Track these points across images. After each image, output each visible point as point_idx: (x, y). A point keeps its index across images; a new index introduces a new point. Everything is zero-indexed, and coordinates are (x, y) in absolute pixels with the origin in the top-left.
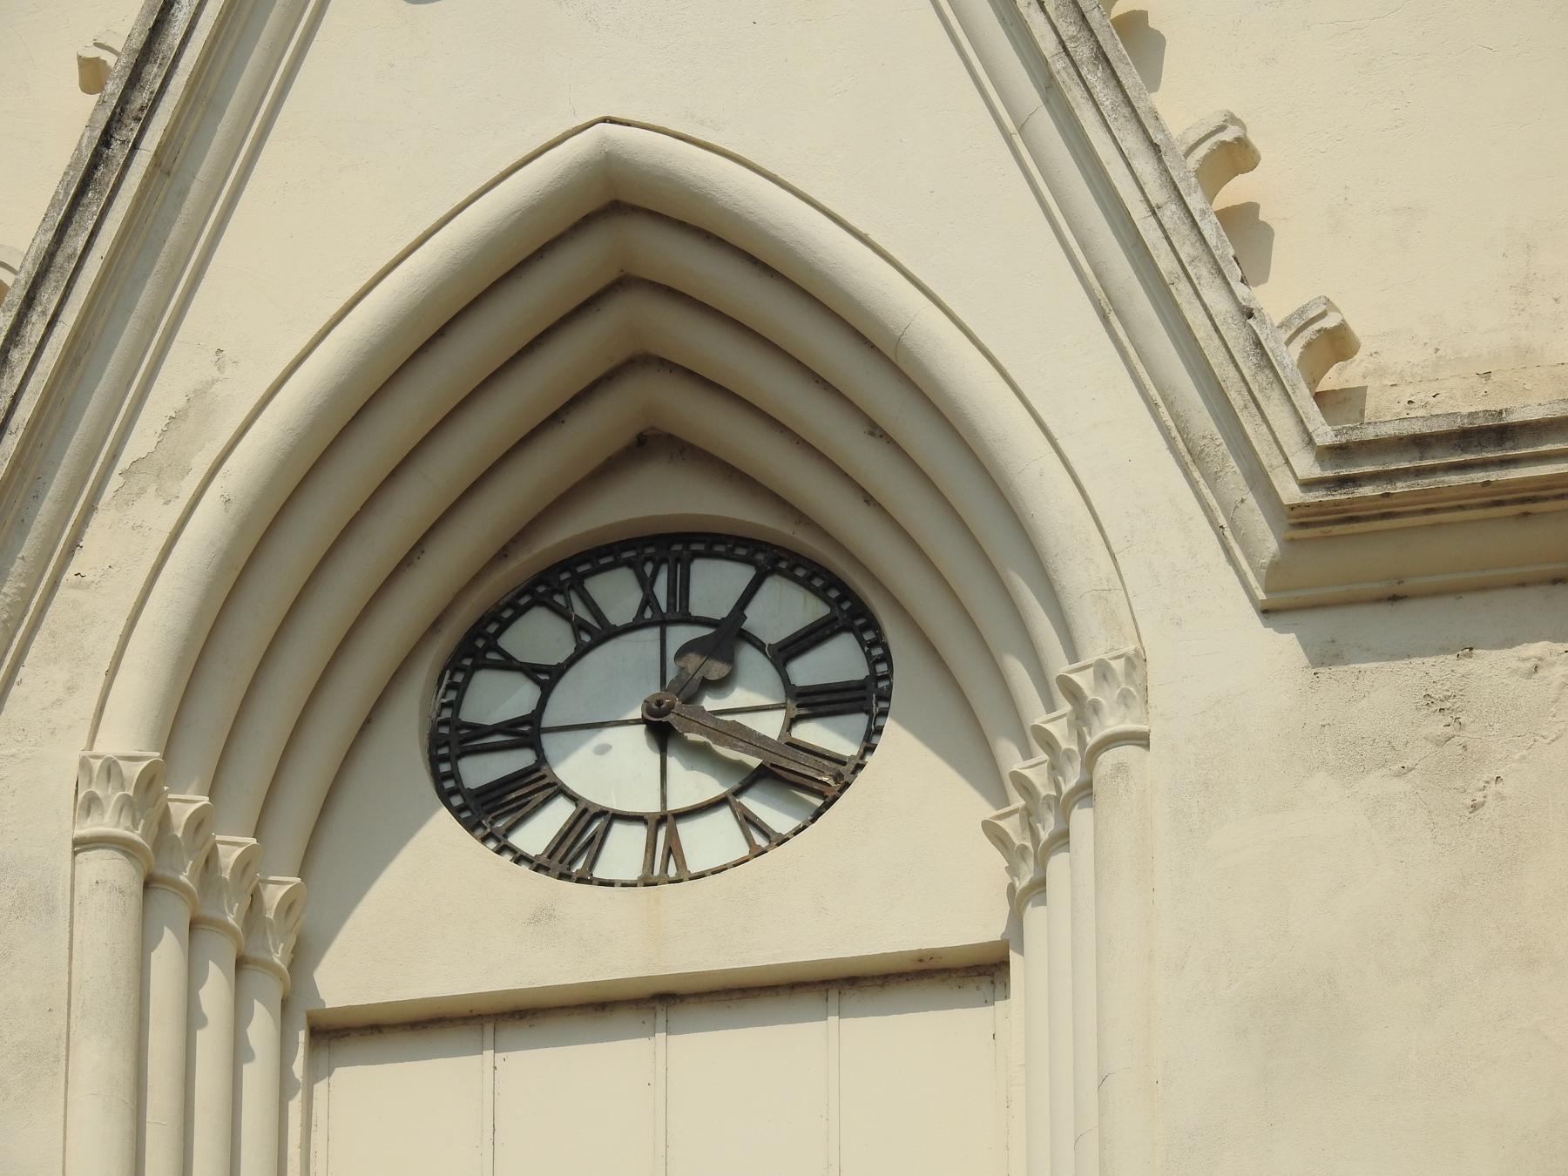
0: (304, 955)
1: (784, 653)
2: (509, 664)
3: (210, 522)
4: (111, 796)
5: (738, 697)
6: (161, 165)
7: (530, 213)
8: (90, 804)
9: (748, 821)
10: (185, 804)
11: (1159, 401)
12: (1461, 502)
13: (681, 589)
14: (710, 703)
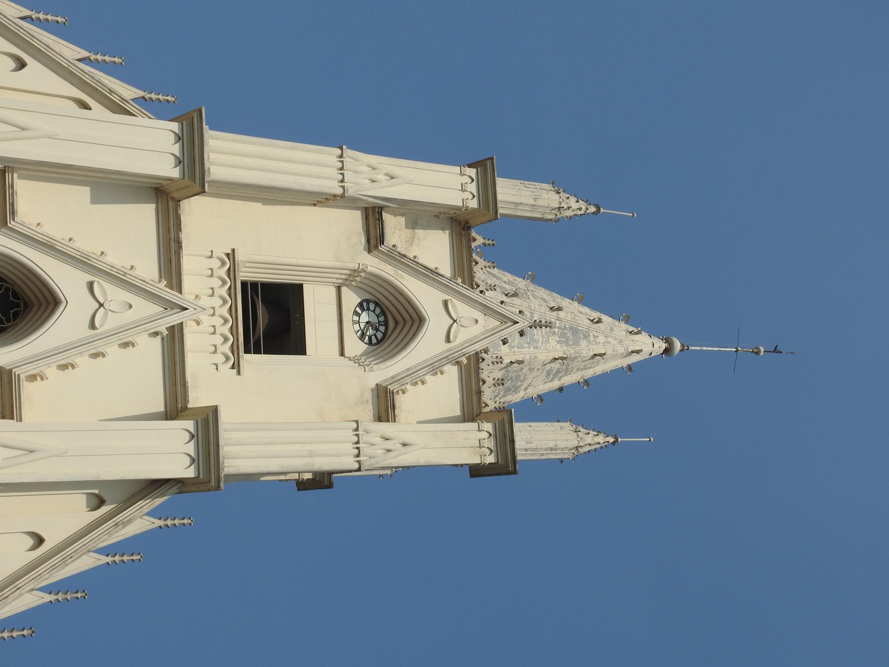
0: (347, 286)
1: (375, 335)
2: (375, 307)
3: (391, 278)
4: (364, 267)
5: (371, 330)
8: (363, 265)
9: (358, 331)
10: (363, 274)
11: (399, 374)
13: (382, 325)
14: (370, 327)
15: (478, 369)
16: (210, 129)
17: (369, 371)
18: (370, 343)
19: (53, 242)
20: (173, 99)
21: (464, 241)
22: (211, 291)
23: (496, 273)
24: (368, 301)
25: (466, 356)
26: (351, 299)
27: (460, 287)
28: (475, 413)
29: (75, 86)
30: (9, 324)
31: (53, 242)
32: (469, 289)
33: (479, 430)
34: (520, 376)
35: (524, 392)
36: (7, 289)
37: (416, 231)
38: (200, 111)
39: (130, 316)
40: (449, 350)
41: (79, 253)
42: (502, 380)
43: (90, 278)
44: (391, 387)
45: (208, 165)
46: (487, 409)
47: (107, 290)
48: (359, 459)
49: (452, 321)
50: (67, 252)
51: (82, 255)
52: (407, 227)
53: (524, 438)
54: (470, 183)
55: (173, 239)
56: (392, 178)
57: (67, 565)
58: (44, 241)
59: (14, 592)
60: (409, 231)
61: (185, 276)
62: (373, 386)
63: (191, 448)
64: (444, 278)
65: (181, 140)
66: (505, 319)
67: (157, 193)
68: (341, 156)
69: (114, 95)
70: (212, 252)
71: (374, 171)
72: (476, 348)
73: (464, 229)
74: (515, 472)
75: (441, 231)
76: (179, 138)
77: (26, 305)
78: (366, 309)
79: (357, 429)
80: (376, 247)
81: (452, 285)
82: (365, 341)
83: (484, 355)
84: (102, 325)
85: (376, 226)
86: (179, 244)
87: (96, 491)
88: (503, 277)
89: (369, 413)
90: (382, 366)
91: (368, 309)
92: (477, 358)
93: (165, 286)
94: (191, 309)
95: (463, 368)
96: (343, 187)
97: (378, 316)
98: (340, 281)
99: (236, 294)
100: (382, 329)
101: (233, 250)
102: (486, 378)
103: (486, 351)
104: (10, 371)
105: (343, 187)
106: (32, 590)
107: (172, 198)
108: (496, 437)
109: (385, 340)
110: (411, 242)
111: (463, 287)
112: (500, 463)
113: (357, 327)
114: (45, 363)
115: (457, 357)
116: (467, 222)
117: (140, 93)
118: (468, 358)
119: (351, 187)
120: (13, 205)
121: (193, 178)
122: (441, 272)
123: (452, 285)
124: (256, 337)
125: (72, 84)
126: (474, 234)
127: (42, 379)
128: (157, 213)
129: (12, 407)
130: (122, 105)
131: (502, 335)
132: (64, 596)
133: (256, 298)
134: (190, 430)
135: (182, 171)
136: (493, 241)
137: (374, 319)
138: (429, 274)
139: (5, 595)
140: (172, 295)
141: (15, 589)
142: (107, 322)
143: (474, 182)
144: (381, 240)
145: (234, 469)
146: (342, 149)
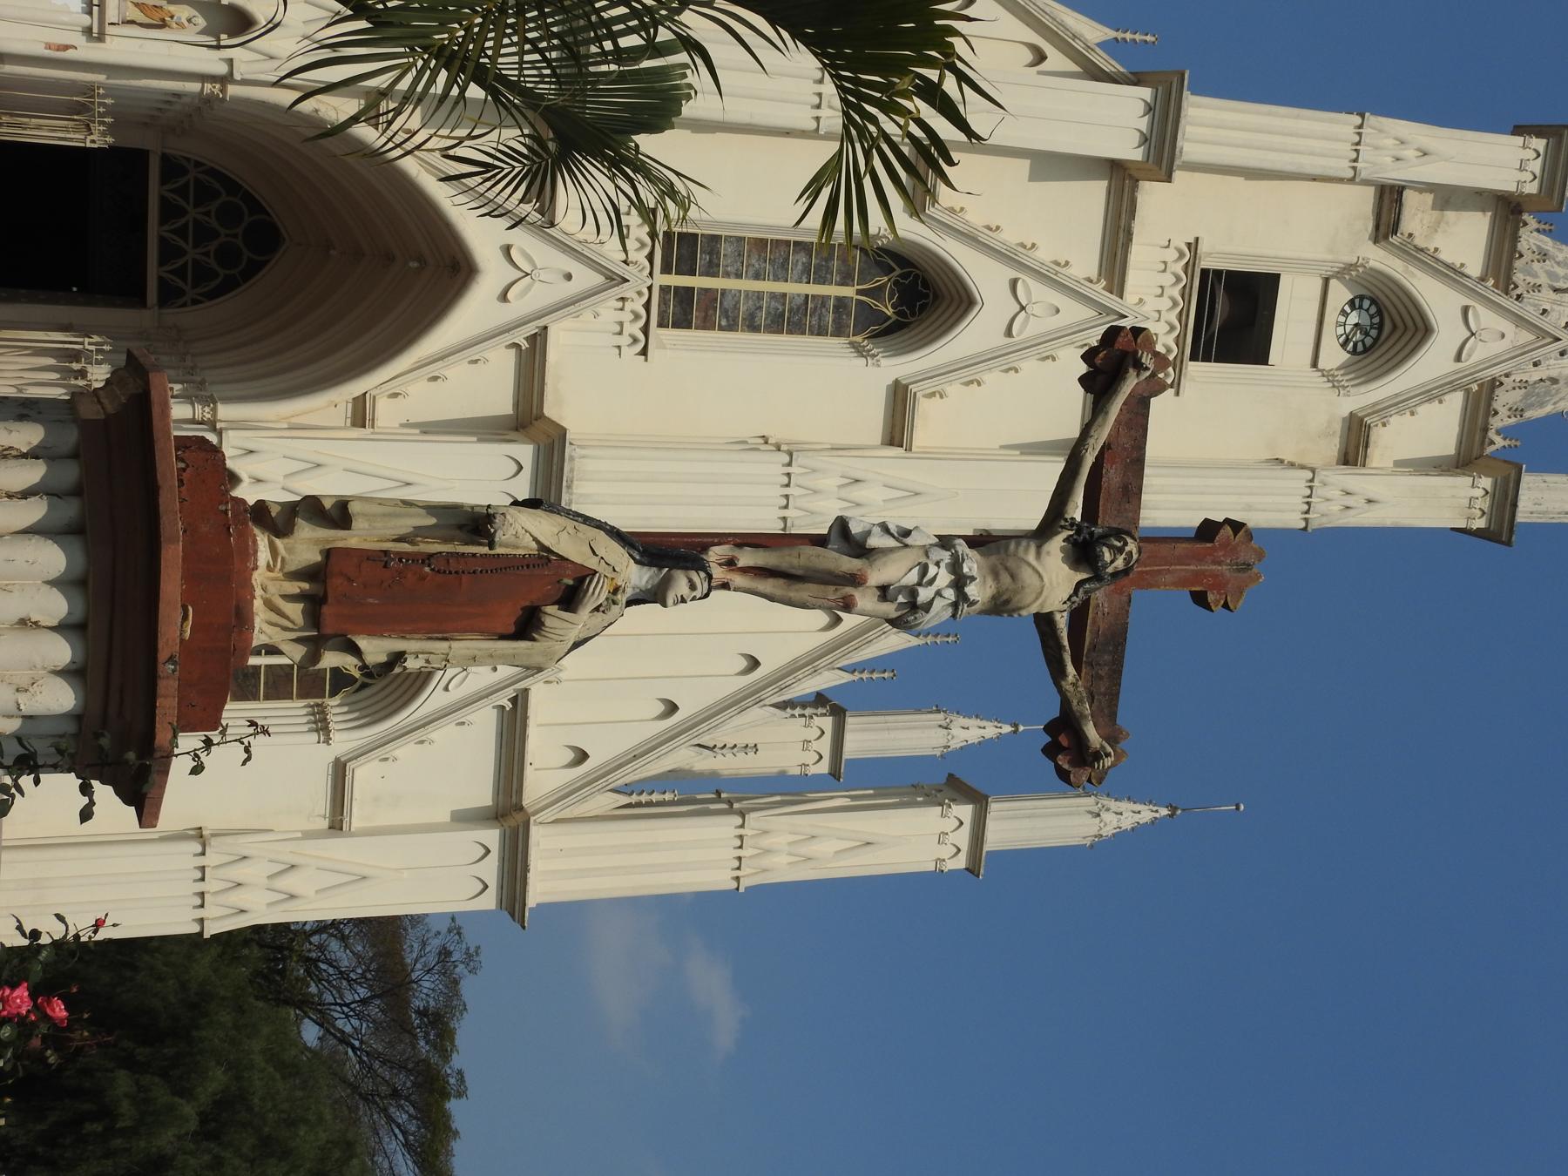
0: (1338, 278)
1: (1363, 341)
2: (1370, 306)
3: (1397, 276)
4: (1364, 262)
5: (1358, 335)
6: (1447, 275)
7: (1428, 320)
8: (1363, 259)
9: (1342, 335)
10: (1361, 270)
11: (1382, 401)
12: (1359, 440)
13: (1375, 328)
14: (1358, 332)
15: (1490, 399)
16: (1192, 94)
17: (1344, 395)
18: (1354, 352)
19: (976, 232)
20: (1153, 39)
21: (1509, 231)
22: (1160, 290)
23: (1551, 249)
24: (1362, 298)
25: (1479, 382)
26: (1340, 295)
27: (1489, 291)
28: (1474, 455)
29: (1031, 28)
30: (913, 319)
31: (976, 232)
32: (1502, 295)
33: (1524, 147)
34: (1551, 391)
35: (1553, 407)
36: (917, 276)
37: (1445, 212)
38: (1183, 75)
39: (1055, 322)
40: (1456, 372)
41: (1005, 247)
42: (1522, 410)
43: (1014, 274)
44: (1368, 420)
45: (1181, 144)
46: (1489, 450)
47: (1033, 290)
48: (1307, 516)
49: (1469, 334)
50: (992, 245)
51: (1009, 249)
52: (1434, 208)
53: (1532, 498)
54: (1531, 182)
55: (1123, 227)
56: (1425, 154)
58: (965, 231)
59: (879, 636)
60: (1436, 213)
61: (1131, 271)
62: (1346, 414)
63: (1143, 124)
64: (1470, 280)
65: (1152, 112)
66: (1541, 333)
67: (1112, 167)
68: (1361, 126)
69: (1078, 41)
70: (1169, 241)
71: (1403, 146)
72: (1494, 372)
73: (1513, 212)
74: (1508, 543)
75: (1480, 214)
76: (1150, 109)
77: (936, 297)
78: (1357, 307)
79: (1312, 480)
80: (1386, 237)
81: (1480, 289)
82: (1348, 349)
83: (1503, 379)
84: (1019, 334)
85: (1391, 209)
88: (1557, 253)
89: (1334, 448)
90: (1363, 389)
91: (1361, 307)
92: (1494, 384)
93: (1103, 288)
94: (1131, 317)
95: (1471, 396)
96: (1354, 168)
97: (1372, 317)
99: (1190, 295)
100: (1374, 333)
102: (1524, 251)
103: (1507, 376)
105: (1354, 168)
107: (1130, 175)
108: (1494, 495)
109: (1377, 346)
110: (1434, 228)
111: (1493, 292)
112: (1492, 528)
113: (1340, 330)
114: (947, 380)
115: (1465, 384)
117: (1111, 34)
118: (1481, 386)
119: (1365, 168)
121: (1159, 162)
122: (1467, 271)
123: (1480, 289)
124: (1210, 333)
125: (1027, 25)
126: (1525, 217)
127: (941, 397)
129: (903, 428)
130: (1087, 54)
131: (1534, 356)
132: (934, 639)
133: (1217, 286)
134: (1142, 130)
135: (1147, 151)
136: (1551, 225)
137: (1366, 321)
138: (1451, 274)
139: (869, 639)
141: (881, 632)
142: (1026, 330)
143: (1540, 158)
144: (1395, 228)
145: (1149, 521)
146: (1363, 116)
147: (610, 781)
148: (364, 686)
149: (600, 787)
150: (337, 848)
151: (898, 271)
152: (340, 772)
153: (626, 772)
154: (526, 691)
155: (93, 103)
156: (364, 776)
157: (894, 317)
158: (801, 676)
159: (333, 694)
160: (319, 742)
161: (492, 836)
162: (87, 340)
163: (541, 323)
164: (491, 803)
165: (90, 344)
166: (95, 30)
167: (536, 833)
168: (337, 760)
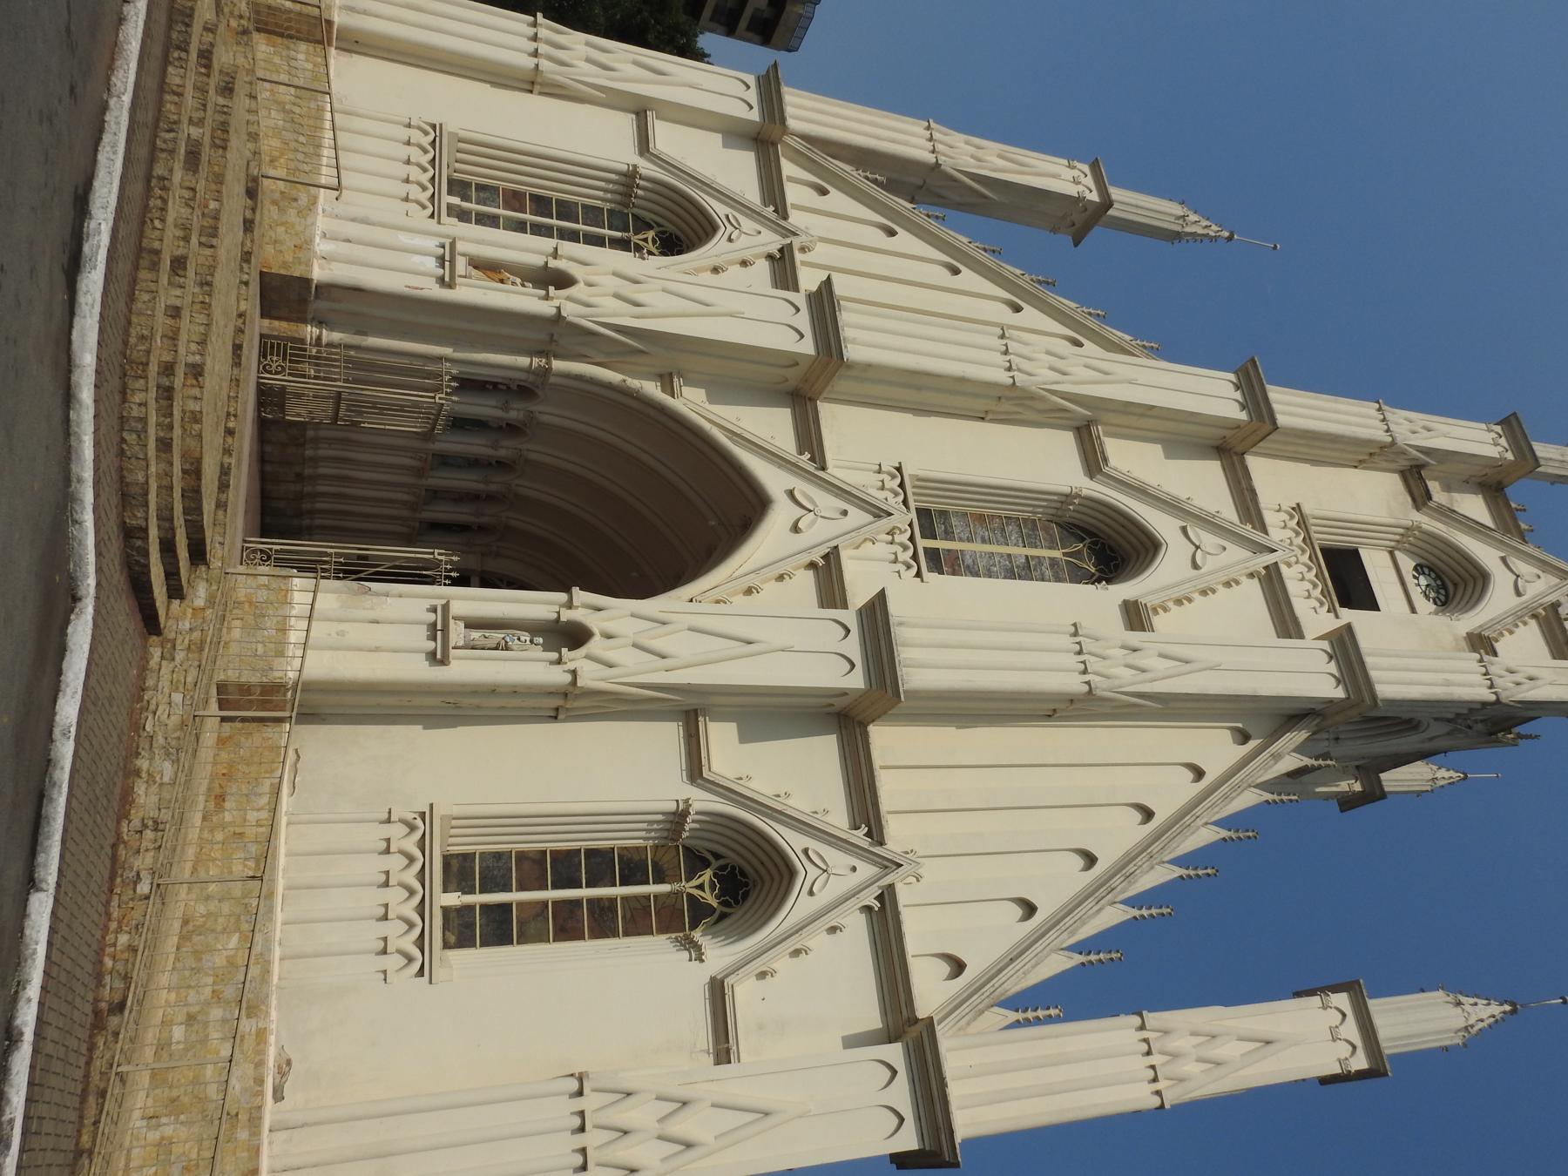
0: (1399, 550)
26: (1407, 564)
38: (1255, 362)
47: (1208, 540)
57: (1233, 798)
77: (1123, 560)
84: (1204, 564)
86: (1253, 492)
87: (1240, 725)
98: (1393, 544)
101: (1298, 504)
104: (1137, 601)
106: (1207, 824)
116: (1500, 483)
120: (1103, 453)
121: (1260, 418)
128: (1224, 469)
140: (1257, 536)
142: (1208, 564)
147: (996, 985)
148: (723, 916)
149: (988, 993)
150: (730, 1083)
151: (1088, 540)
152: (718, 992)
153: (1009, 975)
154: (891, 887)
155: (442, 385)
156: (744, 992)
157: (1098, 574)
158: (1140, 863)
159: (693, 926)
160: (690, 960)
161: (895, 1053)
162: (437, 551)
163: (833, 544)
164: (881, 1026)
165: (439, 554)
166: (447, 279)
167: (945, 1044)
168: (713, 980)
